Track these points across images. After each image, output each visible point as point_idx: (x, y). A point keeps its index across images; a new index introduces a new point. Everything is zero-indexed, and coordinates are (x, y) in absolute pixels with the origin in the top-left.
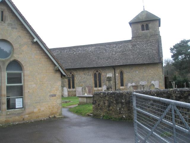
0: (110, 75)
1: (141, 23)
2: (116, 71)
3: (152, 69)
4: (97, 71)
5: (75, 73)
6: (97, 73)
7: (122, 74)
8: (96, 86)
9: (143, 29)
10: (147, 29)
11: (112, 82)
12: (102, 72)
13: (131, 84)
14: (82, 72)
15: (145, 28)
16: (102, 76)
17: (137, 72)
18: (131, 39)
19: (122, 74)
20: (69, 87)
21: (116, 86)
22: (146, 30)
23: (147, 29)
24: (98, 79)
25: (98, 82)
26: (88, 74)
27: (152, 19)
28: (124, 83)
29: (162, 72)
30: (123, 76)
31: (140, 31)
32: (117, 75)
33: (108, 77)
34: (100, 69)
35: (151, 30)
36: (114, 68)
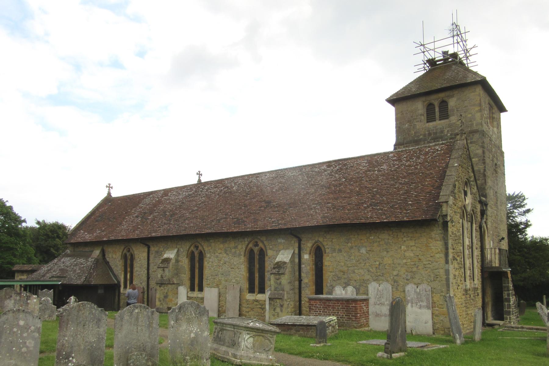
0: (285, 256)
1: (423, 99)
2: (302, 246)
3: (412, 243)
4: (257, 242)
5: (205, 247)
6: (256, 250)
7: (318, 254)
8: (251, 290)
9: (430, 117)
10: (445, 114)
11: (285, 280)
12: (268, 247)
13: (344, 288)
14: (222, 246)
15: (437, 114)
16: (266, 259)
17: (363, 251)
18: (391, 148)
19: (318, 254)
20: (192, 289)
21: (303, 292)
22: (440, 120)
23: (445, 114)
24: (257, 266)
25: (257, 275)
26: (233, 250)
27: (458, 82)
28: (324, 284)
29: (442, 255)
30: (322, 263)
31: (423, 126)
32: (306, 257)
33: (278, 263)
34: (264, 238)
35: (453, 119)
36: (295, 234)
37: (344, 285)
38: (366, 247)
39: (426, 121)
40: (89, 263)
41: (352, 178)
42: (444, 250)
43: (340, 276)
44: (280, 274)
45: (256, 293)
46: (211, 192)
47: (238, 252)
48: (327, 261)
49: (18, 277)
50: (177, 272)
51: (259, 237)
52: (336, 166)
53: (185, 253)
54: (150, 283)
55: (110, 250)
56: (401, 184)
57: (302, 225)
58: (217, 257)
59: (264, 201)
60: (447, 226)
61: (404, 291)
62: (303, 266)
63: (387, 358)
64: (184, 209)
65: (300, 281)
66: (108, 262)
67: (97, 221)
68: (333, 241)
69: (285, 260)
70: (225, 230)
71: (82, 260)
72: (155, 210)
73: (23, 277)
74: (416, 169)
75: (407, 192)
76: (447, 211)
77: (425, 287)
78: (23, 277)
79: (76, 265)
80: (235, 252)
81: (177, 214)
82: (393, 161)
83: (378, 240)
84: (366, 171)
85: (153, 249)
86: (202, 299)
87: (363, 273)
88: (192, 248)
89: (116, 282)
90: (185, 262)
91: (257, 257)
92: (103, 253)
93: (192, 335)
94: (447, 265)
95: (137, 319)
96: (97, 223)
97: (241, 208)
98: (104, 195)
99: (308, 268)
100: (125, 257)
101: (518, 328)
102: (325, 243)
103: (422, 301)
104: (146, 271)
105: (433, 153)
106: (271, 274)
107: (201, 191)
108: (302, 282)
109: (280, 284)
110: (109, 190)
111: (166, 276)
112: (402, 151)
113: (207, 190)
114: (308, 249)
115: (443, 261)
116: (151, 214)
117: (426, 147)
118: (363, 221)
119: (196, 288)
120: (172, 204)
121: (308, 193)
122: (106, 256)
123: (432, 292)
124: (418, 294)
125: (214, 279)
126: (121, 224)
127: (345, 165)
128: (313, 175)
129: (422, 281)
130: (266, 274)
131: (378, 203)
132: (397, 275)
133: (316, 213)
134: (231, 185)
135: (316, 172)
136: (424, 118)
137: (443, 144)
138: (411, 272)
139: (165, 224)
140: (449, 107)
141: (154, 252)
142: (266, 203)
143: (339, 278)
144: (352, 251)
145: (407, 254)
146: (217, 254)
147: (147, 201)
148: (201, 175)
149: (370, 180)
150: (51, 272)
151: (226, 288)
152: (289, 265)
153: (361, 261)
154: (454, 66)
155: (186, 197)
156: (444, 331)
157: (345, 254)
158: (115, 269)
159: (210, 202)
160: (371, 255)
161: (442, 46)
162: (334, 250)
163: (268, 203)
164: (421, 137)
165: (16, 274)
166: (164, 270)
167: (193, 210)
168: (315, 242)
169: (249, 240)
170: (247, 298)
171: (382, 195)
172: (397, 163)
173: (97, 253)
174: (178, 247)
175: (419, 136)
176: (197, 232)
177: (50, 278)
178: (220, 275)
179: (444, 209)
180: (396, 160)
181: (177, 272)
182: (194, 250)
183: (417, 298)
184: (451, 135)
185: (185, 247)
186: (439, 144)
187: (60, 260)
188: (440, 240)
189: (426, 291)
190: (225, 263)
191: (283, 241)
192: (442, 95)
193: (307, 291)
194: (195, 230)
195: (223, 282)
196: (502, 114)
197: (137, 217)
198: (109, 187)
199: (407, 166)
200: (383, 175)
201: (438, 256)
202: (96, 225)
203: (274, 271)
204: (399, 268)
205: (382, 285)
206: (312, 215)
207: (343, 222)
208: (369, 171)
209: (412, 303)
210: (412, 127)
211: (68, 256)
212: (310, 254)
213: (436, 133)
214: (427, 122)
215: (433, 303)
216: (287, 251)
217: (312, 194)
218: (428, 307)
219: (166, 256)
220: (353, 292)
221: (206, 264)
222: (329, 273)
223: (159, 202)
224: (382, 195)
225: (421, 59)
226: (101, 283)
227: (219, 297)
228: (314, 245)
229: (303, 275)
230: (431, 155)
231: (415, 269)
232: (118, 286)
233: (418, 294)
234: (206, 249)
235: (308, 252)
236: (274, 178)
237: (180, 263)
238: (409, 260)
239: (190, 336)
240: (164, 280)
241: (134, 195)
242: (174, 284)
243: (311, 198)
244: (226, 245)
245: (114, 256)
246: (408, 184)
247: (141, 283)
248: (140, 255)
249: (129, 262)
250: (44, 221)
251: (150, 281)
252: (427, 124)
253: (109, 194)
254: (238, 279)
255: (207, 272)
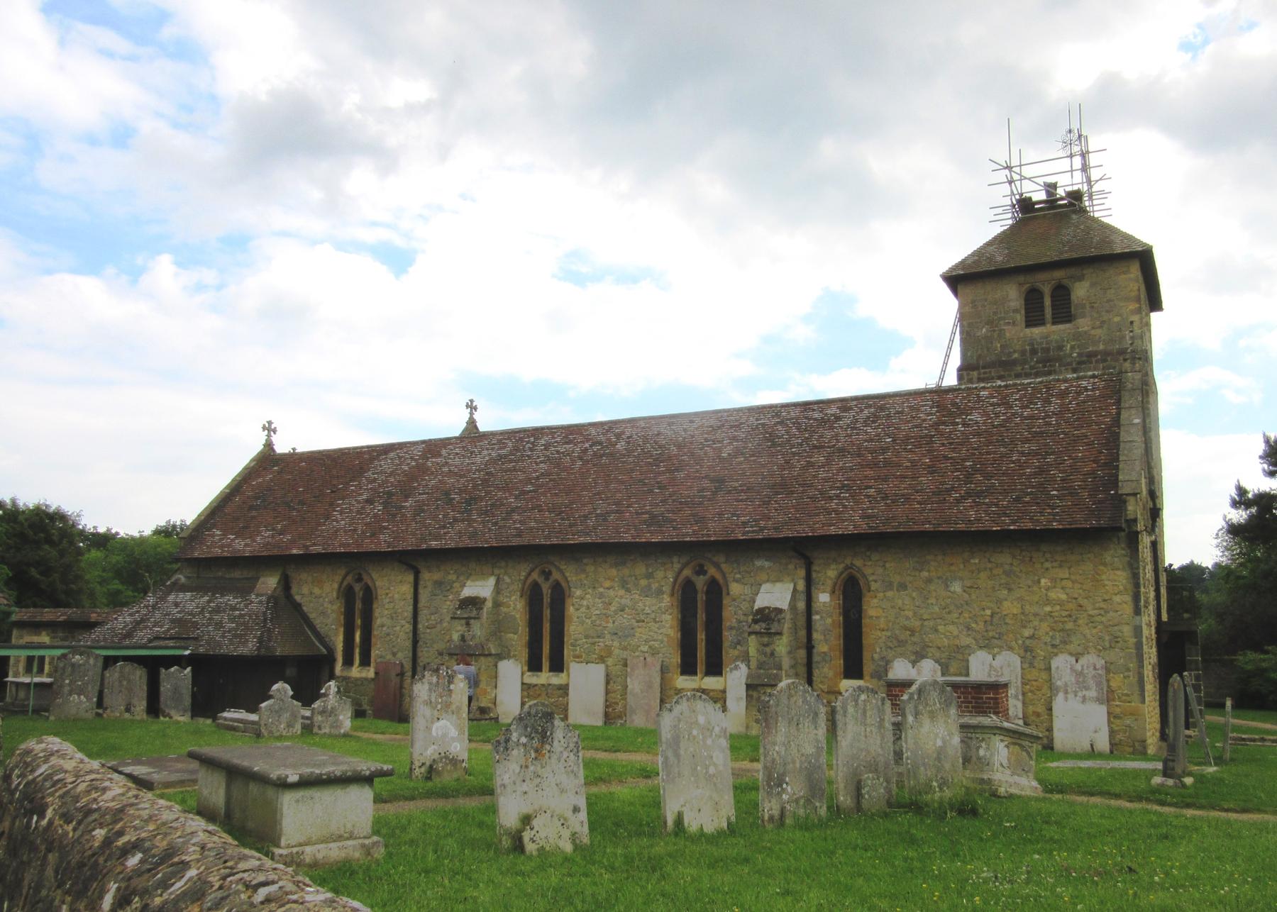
0: (776, 594)
1: (1021, 278)
2: (814, 575)
3: (1064, 573)
4: (701, 566)
5: (569, 573)
6: (700, 582)
7: (852, 596)
8: (688, 668)
9: (1033, 316)
10: (1064, 312)
11: (782, 646)
12: (730, 577)
13: (914, 663)
14: (614, 572)
17: (957, 587)
19: (852, 596)
20: (534, 665)
22: (1054, 323)
23: (1064, 312)
24: (701, 617)
25: (701, 636)
26: (643, 582)
29: (1128, 598)
31: (1019, 334)
32: (823, 598)
33: (761, 610)
34: (721, 558)
35: (1083, 324)
37: (913, 658)
38: (961, 579)
39: (1023, 325)
40: (254, 607)
41: (907, 438)
42: (1130, 587)
43: (902, 637)
44: (770, 634)
45: (699, 675)
46: (558, 452)
47: (655, 586)
48: (875, 609)
49: (21, 637)
50: (499, 626)
51: (709, 556)
52: (862, 411)
53: (517, 586)
54: (420, 654)
55: (304, 576)
56: (1022, 453)
57: (820, 532)
58: (601, 596)
59: (706, 477)
60: (1137, 542)
61: (1049, 669)
62: (816, 617)
63: (1175, 785)
64: (499, 489)
65: (810, 647)
66: (300, 605)
67: (251, 508)
68: (888, 565)
69: (779, 605)
70: (627, 538)
71: (231, 600)
72: (415, 488)
73: (36, 639)
74: (1049, 424)
75: (1041, 471)
76: (1135, 511)
77: (1092, 661)
78: (36, 639)
79: (217, 610)
80: (649, 585)
81: (481, 499)
82: (992, 405)
83: (989, 565)
84: (937, 424)
85: (428, 577)
86: (564, 689)
87: (956, 633)
88: (535, 576)
89: (324, 651)
90: (516, 607)
91: (701, 598)
92: (286, 584)
93: (939, 743)
94: (1138, 618)
95: (865, 712)
96: (254, 513)
97: (651, 491)
98: (257, 447)
99: (829, 621)
100: (347, 595)
101: (1254, 740)
102: (868, 571)
103: (1087, 688)
104: (409, 627)
105: (1079, 393)
106: (750, 634)
107: (531, 450)
108: (815, 651)
109: (772, 654)
110: (269, 436)
111: (474, 637)
112: (1006, 386)
113: (547, 447)
114: (830, 583)
115: (1128, 609)
116: (407, 497)
117: (1058, 380)
118: (961, 526)
119: (546, 664)
120: (461, 476)
121: (810, 464)
122: (294, 590)
123: (1108, 671)
124: (1080, 674)
125: (594, 644)
126: (328, 517)
127: (882, 408)
128: (812, 426)
129: (1086, 648)
130: (725, 633)
131: (983, 492)
132: (1032, 637)
133: (845, 506)
134: (609, 439)
135: (815, 419)
136: (1020, 317)
137: (1094, 377)
138: (1062, 630)
139: (456, 520)
140: (1073, 297)
141: (429, 584)
142: (712, 481)
143: (902, 643)
144: (932, 588)
145: (1052, 595)
146: (601, 590)
147: (385, 464)
148: (476, 409)
149: (951, 444)
150: (146, 627)
151: (625, 665)
152: (788, 616)
153: (952, 608)
154: (1074, 217)
155: (493, 461)
156: (1133, 746)
157: (914, 594)
158: (318, 622)
159: (564, 475)
160: (974, 597)
161: (1048, 171)
162: (890, 586)
163: (720, 481)
164: (1016, 355)
165: (15, 632)
166: (468, 624)
167: (524, 493)
168: (847, 568)
169: (684, 560)
170: (679, 687)
171: (988, 476)
172: (1002, 409)
173: (270, 582)
174: (497, 572)
175: (1010, 354)
176: (555, 541)
177: (150, 641)
178: (608, 636)
179: (1130, 508)
180: (999, 405)
181: (499, 626)
182: (540, 580)
183: (1078, 682)
184: (1080, 355)
185: (518, 574)
186: (1085, 377)
187: (163, 599)
188: (1124, 569)
189: (1095, 668)
190: (622, 610)
191: (767, 564)
192: (1058, 274)
193: (826, 670)
194: (548, 537)
195: (616, 652)
196: (1154, 315)
197: (369, 501)
198: (269, 429)
199: (1026, 418)
200: (977, 434)
201: (1117, 599)
202: (253, 517)
203: (757, 627)
204: (1036, 623)
205: (998, 657)
206: (835, 511)
207: (916, 528)
208: (944, 423)
209: (1066, 692)
210: (996, 335)
211: (183, 588)
212: (833, 592)
213: (1048, 349)
214: (1027, 326)
215: (1111, 691)
216: (778, 585)
217: (823, 466)
218: (1099, 701)
219: (468, 592)
220: (935, 671)
221: (570, 610)
222: (879, 633)
223: (421, 470)
224: (988, 476)
225: (1003, 197)
226: (296, 653)
227: (607, 683)
228: (841, 574)
229: (816, 636)
230: (1075, 399)
231: (1070, 626)
232: (330, 659)
233: (1080, 674)
234: (572, 577)
235: (829, 589)
236: (714, 429)
237: (504, 609)
238: (1058, 607)
239: (934, 744)
240: (469, 646)
241: (341, 450)
242: (490, 655)
243: (822, 475)
244: (626, 571)
245: (317, 591)
246: (1037, 454)
247: (394, 654)
248: (393, 592)
249: (359, 605)
250: (14, 501)
251: (419, 650)
252: (1028, 331)
253: (269, 445)
254: (656, 644)
255: (573, 630)
